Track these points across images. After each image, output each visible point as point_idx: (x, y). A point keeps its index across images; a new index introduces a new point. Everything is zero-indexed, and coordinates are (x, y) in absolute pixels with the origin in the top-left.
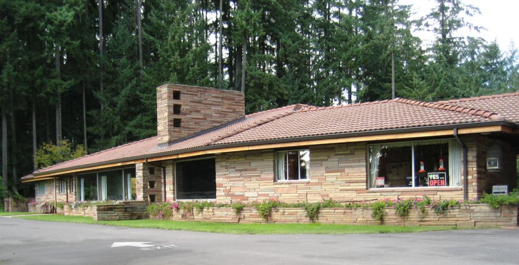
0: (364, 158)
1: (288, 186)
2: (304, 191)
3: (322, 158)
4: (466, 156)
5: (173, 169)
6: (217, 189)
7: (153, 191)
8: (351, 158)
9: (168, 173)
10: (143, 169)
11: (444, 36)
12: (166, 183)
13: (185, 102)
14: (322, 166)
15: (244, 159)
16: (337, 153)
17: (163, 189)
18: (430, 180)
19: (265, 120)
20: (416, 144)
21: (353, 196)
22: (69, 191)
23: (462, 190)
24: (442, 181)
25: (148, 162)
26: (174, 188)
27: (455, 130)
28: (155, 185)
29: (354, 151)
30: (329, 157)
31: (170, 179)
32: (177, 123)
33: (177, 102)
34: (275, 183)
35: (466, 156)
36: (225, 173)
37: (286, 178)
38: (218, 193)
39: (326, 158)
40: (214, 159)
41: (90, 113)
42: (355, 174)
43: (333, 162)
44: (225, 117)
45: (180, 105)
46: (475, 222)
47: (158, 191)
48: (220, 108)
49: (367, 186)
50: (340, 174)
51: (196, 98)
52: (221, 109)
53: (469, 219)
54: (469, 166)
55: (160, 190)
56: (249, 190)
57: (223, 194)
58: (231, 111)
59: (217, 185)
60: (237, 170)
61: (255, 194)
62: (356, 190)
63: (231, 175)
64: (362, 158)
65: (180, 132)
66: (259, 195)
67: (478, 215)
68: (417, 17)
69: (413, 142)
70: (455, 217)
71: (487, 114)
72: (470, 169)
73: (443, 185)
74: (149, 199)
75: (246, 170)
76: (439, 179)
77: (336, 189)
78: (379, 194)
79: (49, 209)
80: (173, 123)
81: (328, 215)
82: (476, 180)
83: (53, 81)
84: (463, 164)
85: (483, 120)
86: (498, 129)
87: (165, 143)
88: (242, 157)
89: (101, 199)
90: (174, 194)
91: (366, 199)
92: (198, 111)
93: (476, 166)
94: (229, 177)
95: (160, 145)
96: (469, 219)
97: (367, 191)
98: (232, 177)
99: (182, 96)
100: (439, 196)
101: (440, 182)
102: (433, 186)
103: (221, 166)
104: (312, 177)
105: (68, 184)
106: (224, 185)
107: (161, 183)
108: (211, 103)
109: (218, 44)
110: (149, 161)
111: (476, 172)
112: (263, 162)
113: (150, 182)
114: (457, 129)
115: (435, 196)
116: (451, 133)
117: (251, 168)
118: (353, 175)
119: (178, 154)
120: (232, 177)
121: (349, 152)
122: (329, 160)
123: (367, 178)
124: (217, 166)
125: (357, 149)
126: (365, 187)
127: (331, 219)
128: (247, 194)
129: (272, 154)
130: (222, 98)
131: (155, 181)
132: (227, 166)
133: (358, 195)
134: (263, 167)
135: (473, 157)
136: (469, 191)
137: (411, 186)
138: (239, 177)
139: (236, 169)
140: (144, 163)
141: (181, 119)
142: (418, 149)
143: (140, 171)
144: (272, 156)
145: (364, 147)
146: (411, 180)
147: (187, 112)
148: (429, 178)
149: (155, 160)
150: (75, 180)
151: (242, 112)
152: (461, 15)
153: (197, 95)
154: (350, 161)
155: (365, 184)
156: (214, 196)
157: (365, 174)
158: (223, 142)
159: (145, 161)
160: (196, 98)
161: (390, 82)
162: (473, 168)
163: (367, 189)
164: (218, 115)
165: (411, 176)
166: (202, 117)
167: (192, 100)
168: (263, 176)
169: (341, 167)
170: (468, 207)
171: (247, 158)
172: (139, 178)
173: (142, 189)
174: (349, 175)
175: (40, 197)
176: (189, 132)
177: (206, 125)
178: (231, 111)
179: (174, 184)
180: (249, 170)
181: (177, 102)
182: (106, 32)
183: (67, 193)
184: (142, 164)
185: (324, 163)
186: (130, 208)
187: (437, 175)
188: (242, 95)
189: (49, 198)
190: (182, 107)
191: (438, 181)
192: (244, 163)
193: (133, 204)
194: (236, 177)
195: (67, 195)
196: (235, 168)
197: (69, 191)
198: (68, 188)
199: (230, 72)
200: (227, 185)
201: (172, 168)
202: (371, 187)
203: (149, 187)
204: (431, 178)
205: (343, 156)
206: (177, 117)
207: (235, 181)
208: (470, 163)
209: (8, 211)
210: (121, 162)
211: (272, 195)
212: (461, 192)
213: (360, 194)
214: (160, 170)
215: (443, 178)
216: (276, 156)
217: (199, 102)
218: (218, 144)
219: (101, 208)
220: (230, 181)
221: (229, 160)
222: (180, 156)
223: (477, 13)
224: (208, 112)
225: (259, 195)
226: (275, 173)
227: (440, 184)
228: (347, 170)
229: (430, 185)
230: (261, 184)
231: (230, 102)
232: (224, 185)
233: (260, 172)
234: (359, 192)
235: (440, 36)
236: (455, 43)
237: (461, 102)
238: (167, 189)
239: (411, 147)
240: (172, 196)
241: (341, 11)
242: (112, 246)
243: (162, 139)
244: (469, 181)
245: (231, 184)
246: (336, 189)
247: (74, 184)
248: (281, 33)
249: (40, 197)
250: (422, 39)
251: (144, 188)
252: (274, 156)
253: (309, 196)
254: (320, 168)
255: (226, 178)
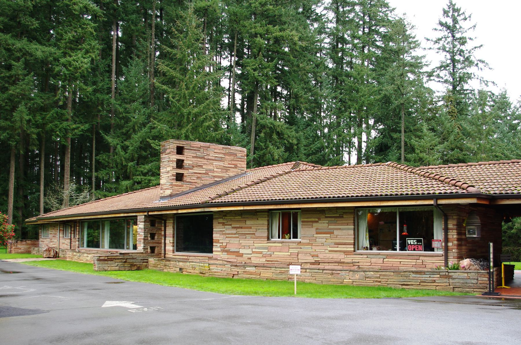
0: (352, 221)
1: (280, 245)
2: (296, 251)
3: (313, 220)
4: (446, 224)
5: (174, 223)
6: (214, 244)
7: (153, 243)
8: (340, 221)
9: (168, 226)
10: (144, 222)
11: (454, 88)
12: (167, 236)
13: (188, 158)
14: (312, 227)
15: (240, 217)
16: (327, 215)
17: (163, 241)
18: (408, 245)
19: (262, 178)
20: (401, 210)
21: (341, 257)
22: (72, 236)
23: (443, 256)
24: (419, 246)
25: (148, 215)
26: (173, 240)
27: (435, 200)
28: (156, 237)
29: (343, 214)
30: (319, 219)
31: (170, 231)
32: (179, 177)
33: (180, 157)
34: (268, 241)
35: (446, 224)
36: (221, 229)
37: (279, 238)
38: (214, 249)
39: (317, 220)
40: (212, 215)
41: (98, 157)
42: (343, 237)
43: (323, 224)
44: (227, 172)
45: (183, 161)
46: (453, 287)
47: (158, 243)
48: (221, 164)
49: (354, 248)
50: (329, 235)
51: (199, 154)
52: (222, 164)
53: (448, 284)
54: (449, 233)
55: (160, 242)
56: (244, 247)
57: (219, 249)
58: (233, 166)
59: (214, 241)
60: (233, 228)
61: (249, 251)
62: (344, 252)
63: (228, 232)
64: (350, 222)
65: (182, 186)
66: (253, 252)
67: (456, 281)
68: (428, 69)
69: (398, 208)
70: (435, 282)
71: (465, 186)
72: (450, 237)
73: (420, 251)
74: (149, 250)
75: (242, 228)
76: (417, 244)
77: (325, 250)
78: (366, 256)
79: (52, 254)
80: (175, 178)
81: (317, 275)
82: (456, 247)
83: (65, 124)
84: (444, 231)
85: (460, 191)
86: (474, 201)
87: (167, 196)
88: (239, 215)
89: (103, 247)
90: (173, 246)
91: (354, 261)
92: (201, 166)
93: (456, 234)
94: (226, 234)
95: (162, 198)
96: (448, 284)
97: (355, 253)
98: (229, 234)
99: (186, 152)
100: (421, 261)
101: (418, 247)
102: (411, 250)
103: (219, 223)
104: (303, 237)
105: (73, 229)
106: (220, 241)
107: (162, 235)
108: (214, 158)
109: (231, 89)
110: (150, 213)
111: (456, 239)
112: (257, 221)
113: (151, 234)
114: (437, 199)
115: (418, 261)
116: (432, 202)
117: (246, 226)
118: (341, 237)
119: (177, 210)
120: (229, 234)
121: (338, 215)
122: (319, 222)
123: (354, 240)
124: (215, 224)
125: (346, 213)
126: (353, 249)
127: (319, 280)
128: (242, 251)
129: (266, 213)
130: (224, 154)
131: (155, 234)
132: (224, 223)
133: (346, 256)
134: (258, 226)
135: (454, 225)
136: (449, 257)
137: (396, 250)
138: (235, 234)
139: (232, 226)
140: (145, 216)
141: (183, 174)
142: (401, 214)
143: (141, 223)
144: (266, 216)
145: (353, 211)
146: (396, 244)
147: (189, 167)
148: (408, 243)
149: (156, 213)
150: (79, 226)
151: (244, 167)
152: (471, 70)
153: (199, 151)
154: (339, 223)
155: (352, 246)
156: (211, 251)
157: (353, 237)
158: (220, 201)
159: (146, 214)
160: (199, 154)
161: (400, 132)
162: (453, 235)
163: (354, 251)
164: (220, 170)
165: (396, 240)
166: (204, 172)
167: (195, 155)
168: (257, 234)
169: (331, 229)
170: (447, 274)
171: (243, 216)
172: (140, 230)
173: (142, 241)
174: (338, 237)
175: (43, 240)
176: (191, 186)
177: (208, 180)
178: (233, 166)
179: (173, 237)
180: (245, 228)
181: (180, 157)
182: (119, 73)
183: (71, 237)
184: (143, 217)
185: (315, 224)
186: (130, 259)
187: (415, 241)
188: (244, 152)
189: (53, 242)
190: (185, 162)
191: (416, 246)
192: (240, 221)
193: (133, 255)
194: (232, 234)
195: (71, 239)
196: (231, 225)
197: (72, 236)
198: (72, 232)
199: (243, 118)
200: (223, 241)
201: (172, 222)
202: (358, 249)
203: (149, 239)
204: (409, 244)
205: (333, 219)
206: (180, 171)
207: (231, 237)
208: (451, 231)
209: (10, 252)
210: (124, 213)
211: (265, 253)
212: (441, 257)
213: (348, 256)
214: (161, 223)
215: (421, 243)
216: (270, 216)
217: (203, 158)
218: (215, 202)
219: (101, 258)
220: (227, 237)
221: (226, 218)
222: (180, 211)
223: (487, 69)
224: (211, 167)
225: (253, 252)
226: (268, 232)
227: (418, 249)
228: (336, 232)
229: (408, 250)
230: (255, 242)
231: (232, 157)
232: (220, 241)
233: (255, 230)
234: (346, 253)
235: (451, 87)
236: (466, 94)
237: (449, 167)
238: (167, 241)
239: (396, 213)
240: (171, 248)
241: (354, 60)
242: (103, 306)
243: (164, 192)
244: (449, 248)
245: (227, 240)
246: (325, 250)
247: (78, 230)
248: (292, 82)
249: (43, 240)
250: (433, 89)
251: (144, 240)
252: (268, 216)
253: (299, 255)
254: (311, 229)
255: (223, 234)
